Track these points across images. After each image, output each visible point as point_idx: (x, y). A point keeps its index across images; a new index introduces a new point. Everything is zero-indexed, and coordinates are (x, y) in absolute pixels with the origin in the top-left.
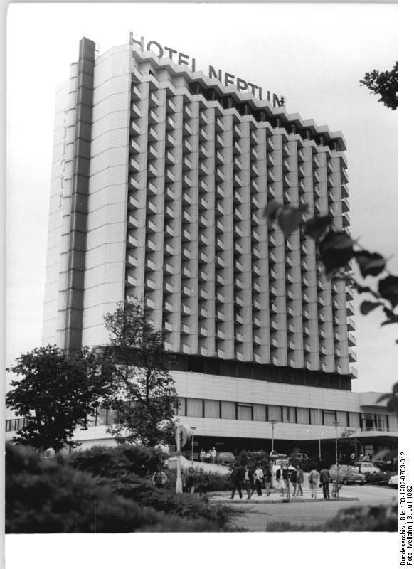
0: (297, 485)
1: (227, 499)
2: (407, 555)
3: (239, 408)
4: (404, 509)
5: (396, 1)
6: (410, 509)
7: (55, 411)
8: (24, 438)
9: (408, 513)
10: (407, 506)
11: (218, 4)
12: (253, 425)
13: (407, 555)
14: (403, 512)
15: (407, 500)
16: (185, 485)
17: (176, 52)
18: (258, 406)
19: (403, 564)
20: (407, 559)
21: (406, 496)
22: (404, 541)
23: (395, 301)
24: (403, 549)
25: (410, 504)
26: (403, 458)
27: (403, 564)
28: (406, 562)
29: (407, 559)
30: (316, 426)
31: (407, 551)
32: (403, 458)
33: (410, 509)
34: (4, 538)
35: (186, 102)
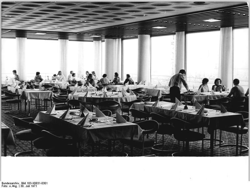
1: (217, 148)
2: (6, 185)
5: (249, 181)
6: (27, 186)
7: (154, 142)
8: (214, 138)
10: (28, 185)
13: (6, 185)
15: (30, 185)
19: (2, 183)
21: (32, 184)
22: (12, 184)
23: (95, 74)
24: (9, 183)
25: (29, 186)
26: (39, 183)
27: (2, 183)
28: (3, 184)
29: (4, 185)
31: (9, 185)
32: (39, 183)
33: (27, 186)
34: (1, 157)
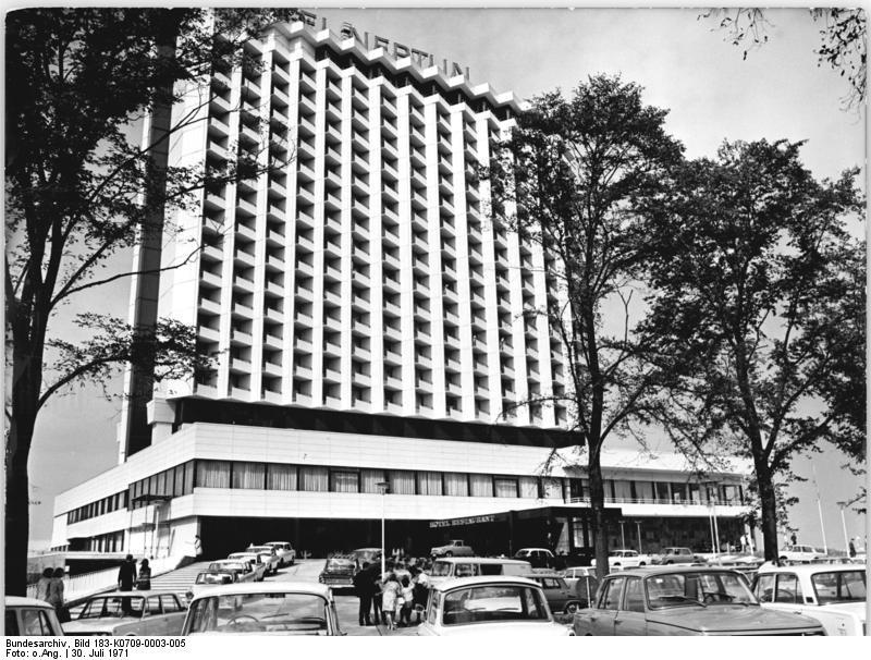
0: (111, 543)
2: (21, 649)
3: (615, 485)
4: (92, 644)
6: (93, 654)
9: (86, 651)
10: (97, 650)
11: (4, 32)
12: (388, 443)
13: (21, 649)
14: (88, 644)
16: (433, 525)
17: (426, 55)
18: (478, 478)
20: (15, 649)
21: (112, 647)
25: (101, 654)
28: (11, 647)
29: (15, 649)
30: (287, 493)
33: (93, 654)
35: (306, 70)
